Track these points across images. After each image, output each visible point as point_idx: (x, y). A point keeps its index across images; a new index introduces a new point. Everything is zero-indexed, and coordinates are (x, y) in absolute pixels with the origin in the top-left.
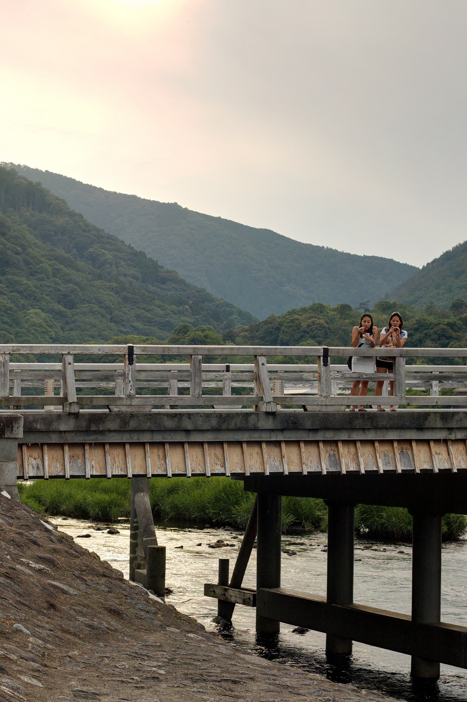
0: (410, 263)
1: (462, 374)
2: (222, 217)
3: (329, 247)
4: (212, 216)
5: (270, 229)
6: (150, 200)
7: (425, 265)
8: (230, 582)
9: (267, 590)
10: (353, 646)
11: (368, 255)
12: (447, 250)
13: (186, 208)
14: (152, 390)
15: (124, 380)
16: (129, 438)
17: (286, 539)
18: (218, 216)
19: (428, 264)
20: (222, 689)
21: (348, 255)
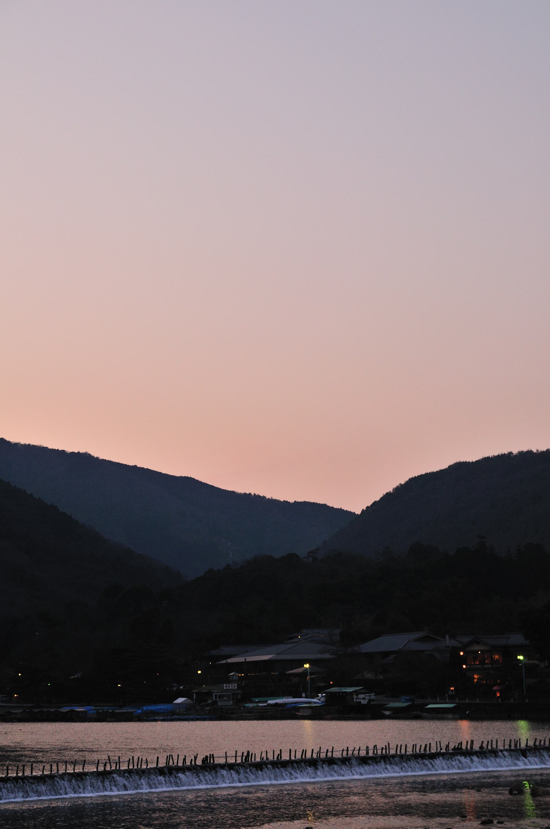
0: (345, 508)
1: (293, 705)
2: (138, 466)
3: (257, 494)
4: (127, 464)
5: (191, 477)
6: (58, 449)
7: (365, 509)
8: (287, 672)
9: (224, 662)
10: (188, 722)
11: (299, 501)
12: (388, 491)
13: (190, 477)
14: (185, 785)
15: (506, 765)
16: (445, 767)
17: (226, 703)
18: (134, 465)
19: (367, 507)
20: (26, 760)
21: (387, 496)
